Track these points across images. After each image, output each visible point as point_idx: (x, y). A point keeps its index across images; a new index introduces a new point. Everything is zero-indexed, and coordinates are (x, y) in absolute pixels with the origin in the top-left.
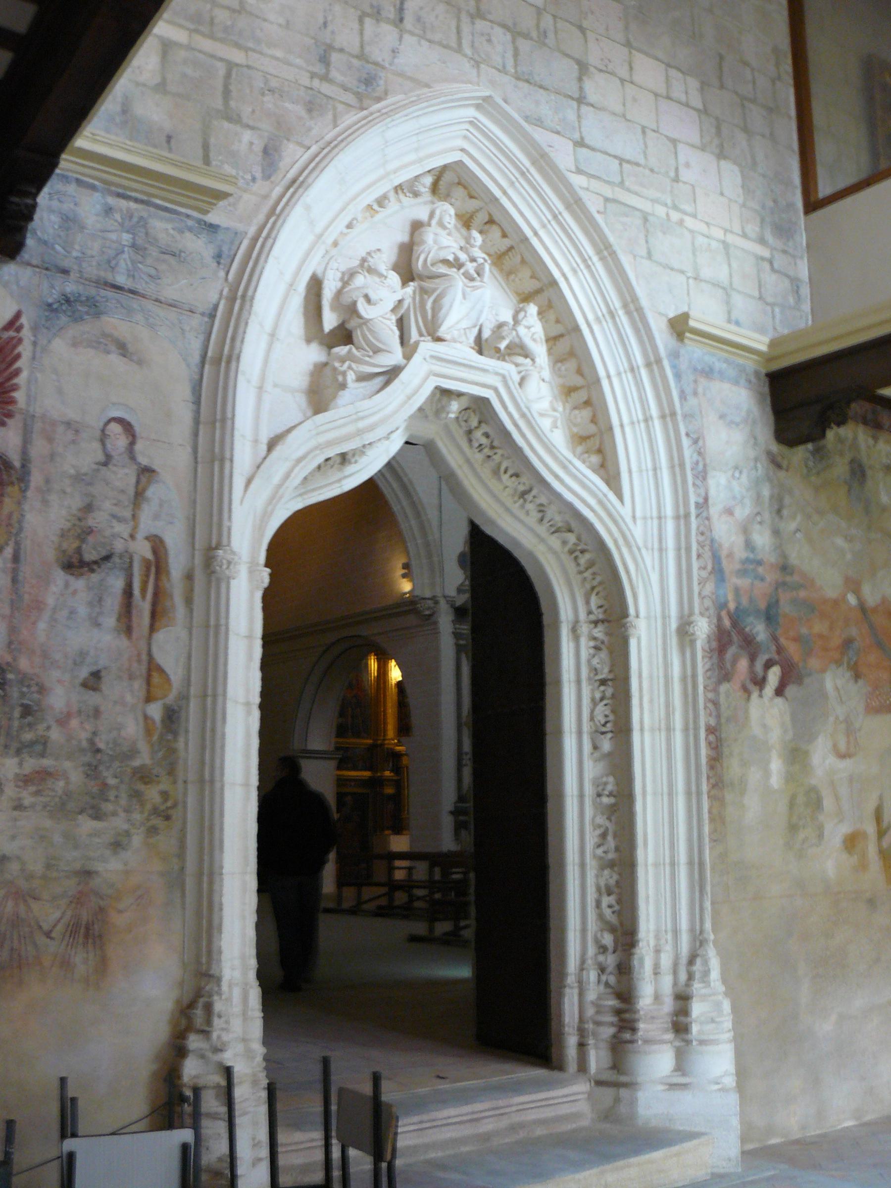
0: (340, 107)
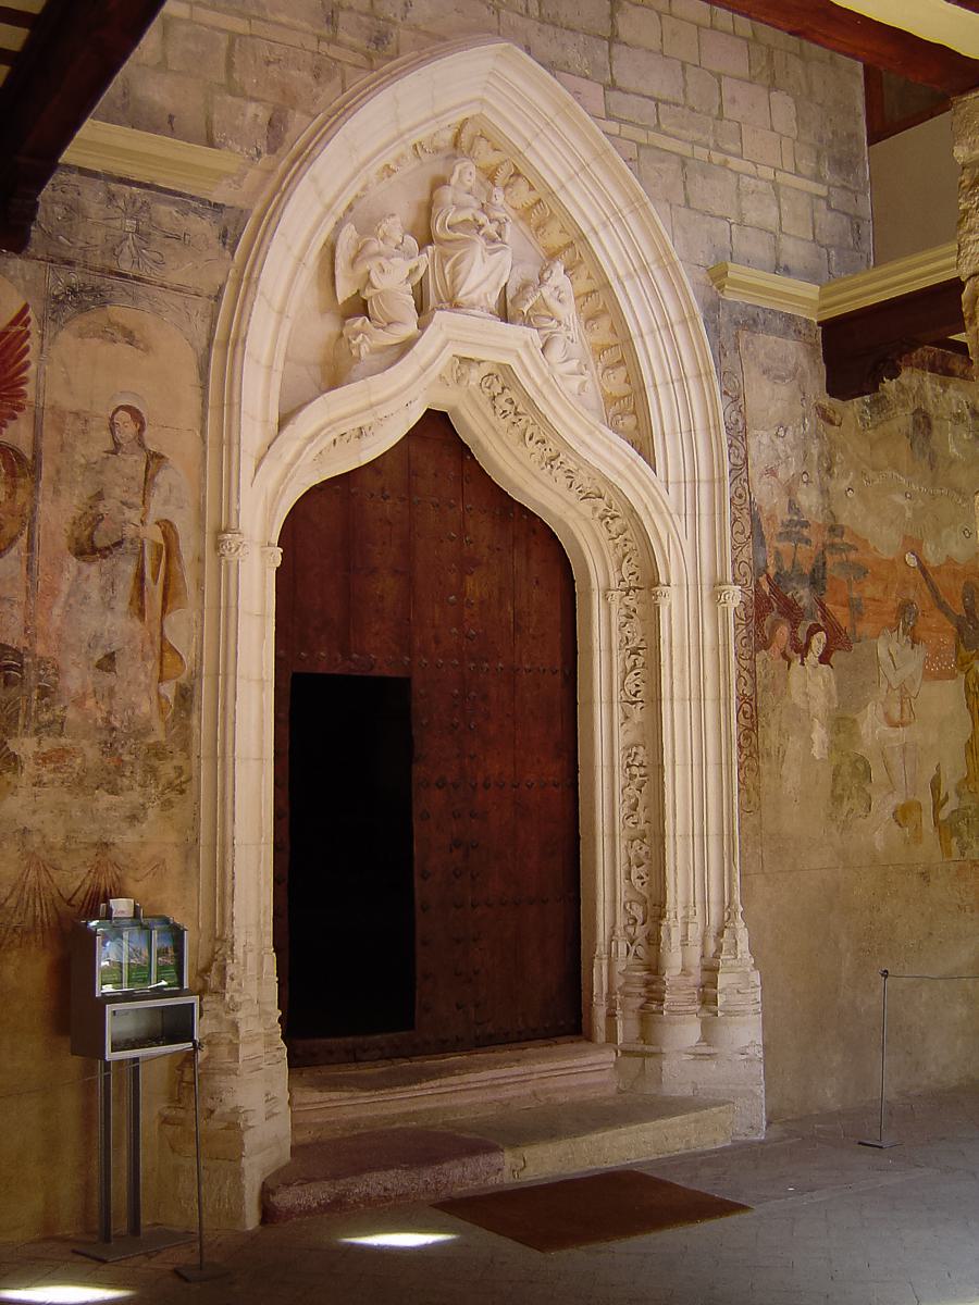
0: (348, 69)
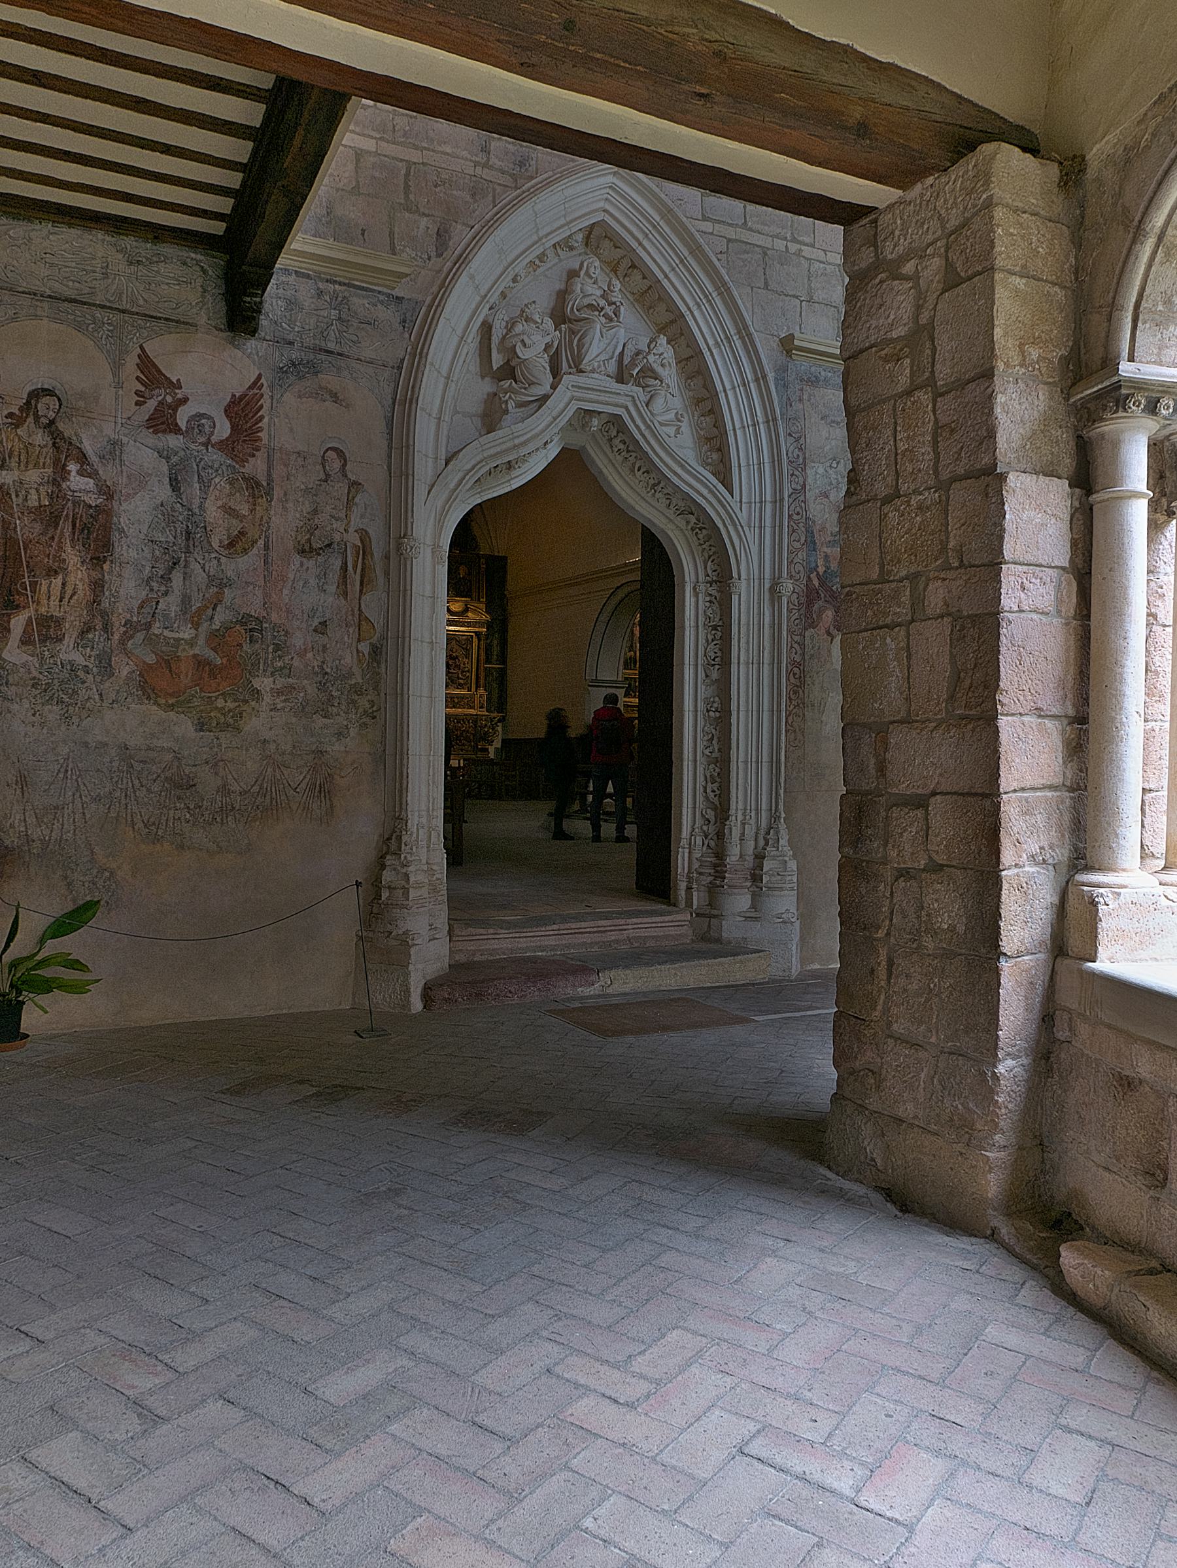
0: (499, 189)
